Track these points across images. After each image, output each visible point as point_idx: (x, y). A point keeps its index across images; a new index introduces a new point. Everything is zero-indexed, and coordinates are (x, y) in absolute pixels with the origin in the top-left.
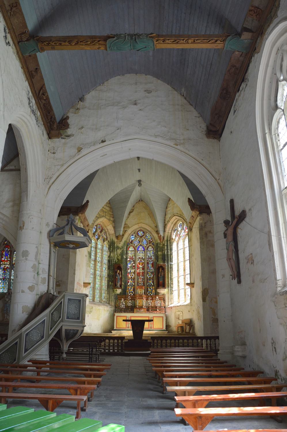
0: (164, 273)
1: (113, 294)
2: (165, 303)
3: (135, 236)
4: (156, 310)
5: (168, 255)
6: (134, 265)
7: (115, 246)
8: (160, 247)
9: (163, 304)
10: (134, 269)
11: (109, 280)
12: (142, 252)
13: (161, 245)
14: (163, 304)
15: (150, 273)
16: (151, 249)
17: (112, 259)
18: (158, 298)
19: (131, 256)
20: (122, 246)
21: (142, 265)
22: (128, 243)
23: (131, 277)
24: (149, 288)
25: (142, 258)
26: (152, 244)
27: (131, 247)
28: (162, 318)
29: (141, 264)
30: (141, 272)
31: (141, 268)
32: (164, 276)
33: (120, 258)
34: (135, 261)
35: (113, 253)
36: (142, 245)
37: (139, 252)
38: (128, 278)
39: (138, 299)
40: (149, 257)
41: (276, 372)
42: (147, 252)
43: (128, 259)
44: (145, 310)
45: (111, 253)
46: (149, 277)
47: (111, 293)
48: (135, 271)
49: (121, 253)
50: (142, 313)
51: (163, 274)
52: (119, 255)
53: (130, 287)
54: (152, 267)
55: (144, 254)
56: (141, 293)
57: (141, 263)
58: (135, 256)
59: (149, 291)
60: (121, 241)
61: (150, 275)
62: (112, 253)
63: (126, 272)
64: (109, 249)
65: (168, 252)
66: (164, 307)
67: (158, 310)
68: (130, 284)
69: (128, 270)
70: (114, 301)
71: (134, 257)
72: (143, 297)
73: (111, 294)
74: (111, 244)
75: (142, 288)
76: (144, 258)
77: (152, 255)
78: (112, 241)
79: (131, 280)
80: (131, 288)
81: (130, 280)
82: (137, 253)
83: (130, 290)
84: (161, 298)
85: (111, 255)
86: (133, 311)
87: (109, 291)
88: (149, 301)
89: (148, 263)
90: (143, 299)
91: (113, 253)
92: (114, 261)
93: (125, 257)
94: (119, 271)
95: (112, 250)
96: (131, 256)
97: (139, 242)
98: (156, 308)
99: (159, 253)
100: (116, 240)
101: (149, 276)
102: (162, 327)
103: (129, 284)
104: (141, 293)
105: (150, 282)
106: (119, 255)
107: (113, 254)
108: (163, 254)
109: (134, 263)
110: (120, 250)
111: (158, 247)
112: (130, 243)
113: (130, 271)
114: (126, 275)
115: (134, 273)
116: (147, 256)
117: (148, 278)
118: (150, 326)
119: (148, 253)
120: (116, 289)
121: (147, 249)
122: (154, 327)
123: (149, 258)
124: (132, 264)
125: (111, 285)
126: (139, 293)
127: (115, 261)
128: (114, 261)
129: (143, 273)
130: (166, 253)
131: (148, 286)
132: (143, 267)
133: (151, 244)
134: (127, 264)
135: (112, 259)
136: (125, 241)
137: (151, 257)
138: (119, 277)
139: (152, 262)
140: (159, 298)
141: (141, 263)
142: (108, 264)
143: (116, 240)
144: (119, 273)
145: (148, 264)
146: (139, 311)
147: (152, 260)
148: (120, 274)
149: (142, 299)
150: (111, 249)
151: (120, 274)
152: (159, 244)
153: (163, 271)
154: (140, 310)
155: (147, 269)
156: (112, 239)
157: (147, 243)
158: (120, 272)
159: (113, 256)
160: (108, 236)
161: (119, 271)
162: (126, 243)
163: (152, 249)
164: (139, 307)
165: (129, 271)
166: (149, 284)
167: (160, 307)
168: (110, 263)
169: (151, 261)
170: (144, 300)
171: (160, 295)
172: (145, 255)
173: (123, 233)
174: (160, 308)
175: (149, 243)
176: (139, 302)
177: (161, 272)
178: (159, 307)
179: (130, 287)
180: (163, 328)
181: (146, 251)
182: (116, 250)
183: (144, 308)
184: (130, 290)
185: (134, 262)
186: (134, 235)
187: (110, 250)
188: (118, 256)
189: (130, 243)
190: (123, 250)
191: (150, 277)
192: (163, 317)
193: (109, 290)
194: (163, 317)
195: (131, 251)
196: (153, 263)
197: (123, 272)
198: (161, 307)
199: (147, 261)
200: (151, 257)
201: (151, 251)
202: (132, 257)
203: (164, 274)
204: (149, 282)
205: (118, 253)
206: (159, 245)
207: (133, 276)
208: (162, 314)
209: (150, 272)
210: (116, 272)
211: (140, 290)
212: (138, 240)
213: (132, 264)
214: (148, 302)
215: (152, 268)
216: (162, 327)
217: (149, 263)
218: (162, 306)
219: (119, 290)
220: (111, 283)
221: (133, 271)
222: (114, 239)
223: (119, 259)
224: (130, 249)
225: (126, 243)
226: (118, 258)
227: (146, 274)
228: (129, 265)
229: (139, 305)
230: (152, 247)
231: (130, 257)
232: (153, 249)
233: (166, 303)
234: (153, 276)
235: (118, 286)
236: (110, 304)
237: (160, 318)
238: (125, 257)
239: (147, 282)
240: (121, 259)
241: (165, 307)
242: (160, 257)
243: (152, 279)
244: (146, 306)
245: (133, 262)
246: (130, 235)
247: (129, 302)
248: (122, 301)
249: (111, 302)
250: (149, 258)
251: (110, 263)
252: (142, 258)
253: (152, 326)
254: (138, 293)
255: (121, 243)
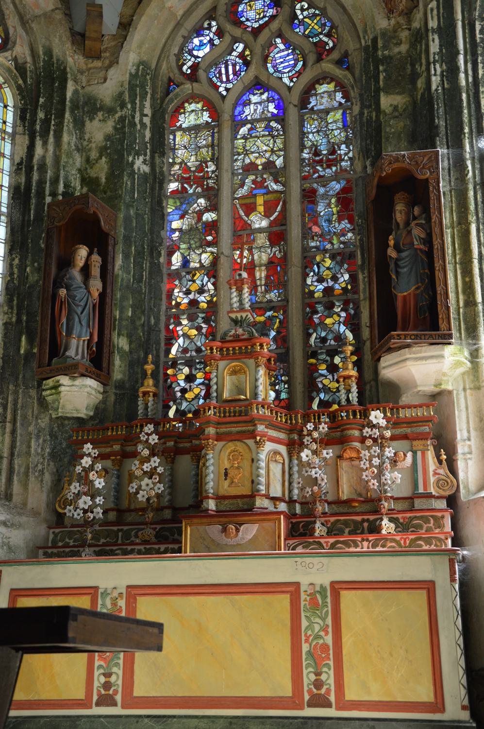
0: (429, 219)
1: (44, 422)
2: (453, 470)
3: (220, 33)
4: (375, 529)
5: (452, 92)
6: (208, 217)
7: (69, 94)
8: (387, 60)
9: (432, 479)
10: (209, 244)
11: (19, 320)
12: (268, 128)
13: (399, 43)
14: (432, 479)
15: (328, 262)
16: (331, 95)
17: (41, 183)
18: (383, 423)
19: (192, 162)
20: (121, 94)
21: (267, 215)
22: (170, 80)
23: (194, 303)
24: (323, 369)
25: (269, 165)
26: (339, 63)
27: (190, 107)
28: (421, 596)
29: (261, 209)
30: (265, 258)
31: (260, 230)
32: (430, 254)
33: (101, 170)
34: (217, 196)
35: (51, 139)
36: (263, 78)
37: (244, 130)
38: (170, 307)
39: (219, 437)
40: (317, 153)
41: (468, 574)
42: (302, 125)
43: (173, 186)
44: (268, 525)
45: (39, 143)
46: (321, 287)
47: (24, 417)
48: (215, 262)
49: (108, 138)
50: (240, 552)
51: (417, 232)
52: (94, 155)
53: (186, 370)
54: (340, 220)
55: (279, 141)
56: (240, 390)
57: (260, 200)
58: (216, 160)
59: (326, 389)
60: (114, 61)
61: (327, 274)
62: (45, 143)
63: (156, 270)
64: (23, 118)
65: (452, 72)
66: (443, 504)
67: (387, 526)
68: (185, 350)
69: (171, 254)
70: (47, 478)
71: (212, 167)
72: (252, 422)
73: (26, 423)
74: (38, 83)
75: (252, 354)
76: (279, 162)
77: (338, 135)
78: (49, 63)
79: (191, 319)
80: (190, 378)
81: (185, 322)
82: (234, 138)
83: (184, 391)
84: (411, 422)
85: (39, 151)
86: (176, 546)
87: (15, 403)
88: (305, 455)
89: (314, 191)
90: (252, 435)
91: (51, 139)
92: (54, 194)
93: (140, 165)
94: (83, 252)
95: (46, 122)
96: (192, 162)
97: (247, 63)
98: (377, 511)
99: (386, 102)
100: (74, 60)
101: (321, 280)
102: (424, 693)
103: (174, 350)
104: (240, 390)
105: (328, 321)
106: (94, 155)
107: (51, 148)
108: (414, 103)
109: (213, 207)
110: (104, 120)
111: (377, 62)
112: (181, 79)
113: (186, 262)
114: (155, 291)
115: (212, 271)
116: (302, 147)
117: (312, 293)
118: (308, 677)
119: (311, 127)
120: (50, 382)
121: (304, 102)
122: (351, 695)
123: (320, 162)
124: (200, 214)
125: (29, 355)
126: (226, 395)
127: (61, 188)
128: (54, 194)
129: (271, 264)
130: (435, 81)
131: (314, 355)
132: (271, 224)
133: (327, 66)
134: (159, 217)
135: (41, 183)
136: (142, 63)
137: (333, 152)
138: (80, 293)
139: (336, 186)
140: (395, 423)
141: (260, 200)
142: (17, 216)
143: (74, 60)
144: (86, 270)
145: (314, 202)
146: (223, 539)
147: (343, 170)
148: (96, 271)
149: (250, 442)
150: (41, 115)
151: (96, 271)
152: (380, 44)
153: (417, 210)
154: (225, 530)
155: (306, 234)
156: (49, 52)
157: (300, 64)
158: (96, 259)
159: (49, 161)
160: (11, 31)
161: (90, 254)
162: (154, 78)
163: (339, 96)
164: (226, 505)
165: (176, 260)
166: (324, 340)
167: (411, 499)
168: (26, 209)
169: (336, 178)
170: (269, 446)
171: (405, 400)
172: (285, 149)
173: (129, 11)
174: (412, 509)
175: (311, 58)
176: (227, 465)
177: (407, 224)
178: (400, 506)
179: (186, 370)
180: (438, 705)
181: (293, 114)
182: (79, 125)
183: (265, 514)
184: (184, 391)
185: (208, 198)
186: (210, 27)
187: (33, 122)
188: (88, 160)
189: (178, 78)
190: (122, 119)
191: (328, 291)
192: (429, 587)
193: (16, 393)
194: (429, 587)
195: (189, 129)
196: (344, 190)
197: (119, 261)
198: (418, 504)
199: (305, 178)
200: (333, 152)
201: (327, 112)
202: (200, 169)
203: (430, 235)
204: (325, 327)
205: (90, 141)
206: (385, 47)
207: (201, 291)
208: (425, 560)
209: (325, 251)
210: (66, 262)
211: (234, 372)
212: (241, 56)
213: (200, 214)
214: (301, 464)
215: (345, 224)
216: (424, 693)
217: (322, 190)
218: (429, 496)
219: (80, 381)
220: (30, 341)
221: (206, 258)
222: (57, 51)
223: (97, 179)
224: (186, 120)
225: (154, 78)
226: (93, 173)
227: (295, 271)
228: (175, 225)
229: (226, 488)
230: (341, 86)
231: (187, 169)
232: (346, 96)
233: (460, 465)
234: (353, 279)
235: (71, 353)
236: (15, 498)
237: (403, 595)
238: (146, 169)
239: (308, 325)
240: (111, 176)
241: (452, 501)
242: (394, 127)
243: (346, 303)
244: (291, 502)
245: (202, 201)
246: (183, 32)
247: (146, 467)
248: (86, 462)
249: (25, 485)
250: (313, 164)
251: (26, 209)
252: (269, 165)
253: (328, 677)
254: (219, 392)
255: (112, 72)
